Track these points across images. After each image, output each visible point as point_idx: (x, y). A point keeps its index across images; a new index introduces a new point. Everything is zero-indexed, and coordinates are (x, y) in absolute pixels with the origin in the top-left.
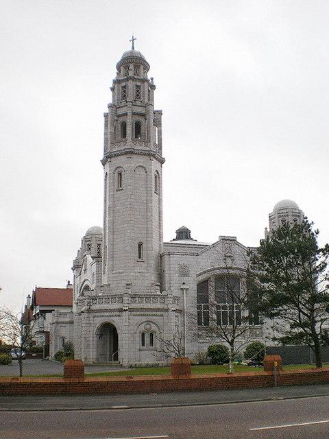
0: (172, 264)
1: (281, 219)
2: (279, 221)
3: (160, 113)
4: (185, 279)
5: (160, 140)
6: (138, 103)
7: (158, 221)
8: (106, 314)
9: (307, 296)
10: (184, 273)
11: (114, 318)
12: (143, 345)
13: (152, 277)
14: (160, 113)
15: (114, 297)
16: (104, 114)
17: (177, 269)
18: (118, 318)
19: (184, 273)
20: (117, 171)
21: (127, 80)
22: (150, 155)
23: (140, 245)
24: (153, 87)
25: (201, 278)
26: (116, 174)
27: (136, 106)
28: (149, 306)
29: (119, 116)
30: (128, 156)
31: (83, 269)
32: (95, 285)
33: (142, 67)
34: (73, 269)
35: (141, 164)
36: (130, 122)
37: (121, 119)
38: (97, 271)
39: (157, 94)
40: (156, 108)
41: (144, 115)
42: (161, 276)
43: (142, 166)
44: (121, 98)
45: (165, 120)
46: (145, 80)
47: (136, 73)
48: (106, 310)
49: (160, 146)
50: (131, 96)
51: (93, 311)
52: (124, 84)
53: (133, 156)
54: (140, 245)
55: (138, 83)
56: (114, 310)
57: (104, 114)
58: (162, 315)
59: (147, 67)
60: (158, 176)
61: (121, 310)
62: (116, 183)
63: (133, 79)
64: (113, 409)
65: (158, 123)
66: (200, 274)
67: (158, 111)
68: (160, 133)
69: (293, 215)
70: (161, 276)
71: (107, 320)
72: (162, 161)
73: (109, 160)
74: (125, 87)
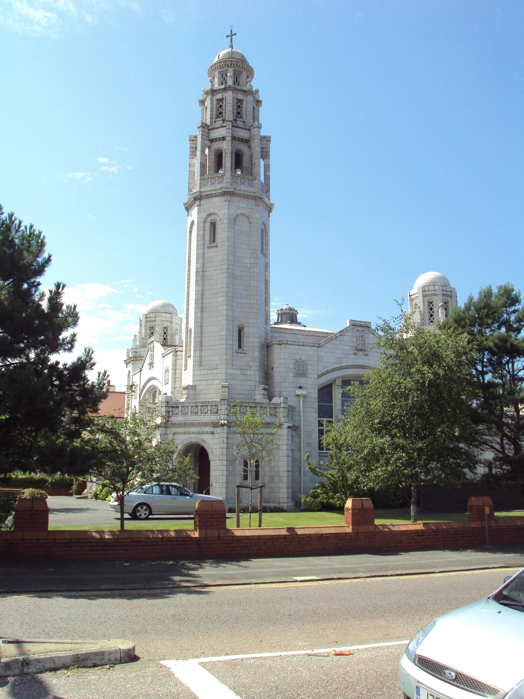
0: (282, 358)
1: (427, 299)
2: (424, 302)
3: (267, 139)
4: (302, 381)
5: (267, 178)
6: (239, 123)
7: (264, 294)
8: (193, 429)
9: (75, 414)
10: (301, 370)
11: (205, 437)
12: (245, 478)
13: (255, 374)
14: (267, 139)
15: (204, 405)
16: (190, 136)
17: (292, 366)
18: (211, 436)
19: (301, 370)
20: (209, 220)
21: (225, 90)
22: (257, 199)
23: (240, 331)
24: (258, 102)
25: (324, 380)
26: (208, 225)
27: (237, 127)
28: (192, 418)
29: (212, 141)
30: (227, 198)
31: (148, 361)
32: (169, 386)
33: (245, 74)
34: (127, 363)
35: (243, 211)
36: (226, 146)
37: (216, 145)
38: (175, 366)
39: (263, 112)
40: (263, 132)
41: (247, 141)
42: (267, 377)
43: (244, 215)
44: (214, 116)
45: (275, 149)
46: (248, 93)
47: (236, 81)
48: (192, 425)
49: (266, 187)
50: (229, 112)
51: (175, 425)
52: (219, 96)
53: (235, 199)
54: (240, 331)
55: (240, 97)
56: (206, 424)
57: (190, 136)
58: (213, 433)
59: (250, 73)
60: (264, 232)
61: (216, 425)
62: (207, 238)
63: (235, 90)
64: (296, 581)
65: (265, 154)
66: (323, 375)
67: (265, 137)
68: (267, 168)
69: (443, 295)
70: (267, 377)
71: (194, 439)
72: (270, 209)
73: (197, 203)
74: (221, 100)
